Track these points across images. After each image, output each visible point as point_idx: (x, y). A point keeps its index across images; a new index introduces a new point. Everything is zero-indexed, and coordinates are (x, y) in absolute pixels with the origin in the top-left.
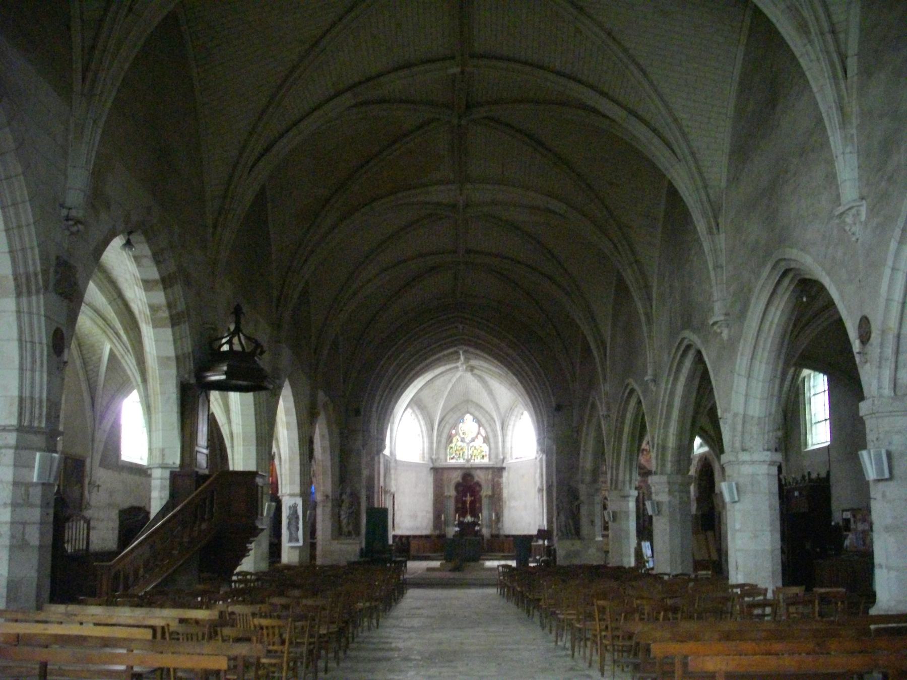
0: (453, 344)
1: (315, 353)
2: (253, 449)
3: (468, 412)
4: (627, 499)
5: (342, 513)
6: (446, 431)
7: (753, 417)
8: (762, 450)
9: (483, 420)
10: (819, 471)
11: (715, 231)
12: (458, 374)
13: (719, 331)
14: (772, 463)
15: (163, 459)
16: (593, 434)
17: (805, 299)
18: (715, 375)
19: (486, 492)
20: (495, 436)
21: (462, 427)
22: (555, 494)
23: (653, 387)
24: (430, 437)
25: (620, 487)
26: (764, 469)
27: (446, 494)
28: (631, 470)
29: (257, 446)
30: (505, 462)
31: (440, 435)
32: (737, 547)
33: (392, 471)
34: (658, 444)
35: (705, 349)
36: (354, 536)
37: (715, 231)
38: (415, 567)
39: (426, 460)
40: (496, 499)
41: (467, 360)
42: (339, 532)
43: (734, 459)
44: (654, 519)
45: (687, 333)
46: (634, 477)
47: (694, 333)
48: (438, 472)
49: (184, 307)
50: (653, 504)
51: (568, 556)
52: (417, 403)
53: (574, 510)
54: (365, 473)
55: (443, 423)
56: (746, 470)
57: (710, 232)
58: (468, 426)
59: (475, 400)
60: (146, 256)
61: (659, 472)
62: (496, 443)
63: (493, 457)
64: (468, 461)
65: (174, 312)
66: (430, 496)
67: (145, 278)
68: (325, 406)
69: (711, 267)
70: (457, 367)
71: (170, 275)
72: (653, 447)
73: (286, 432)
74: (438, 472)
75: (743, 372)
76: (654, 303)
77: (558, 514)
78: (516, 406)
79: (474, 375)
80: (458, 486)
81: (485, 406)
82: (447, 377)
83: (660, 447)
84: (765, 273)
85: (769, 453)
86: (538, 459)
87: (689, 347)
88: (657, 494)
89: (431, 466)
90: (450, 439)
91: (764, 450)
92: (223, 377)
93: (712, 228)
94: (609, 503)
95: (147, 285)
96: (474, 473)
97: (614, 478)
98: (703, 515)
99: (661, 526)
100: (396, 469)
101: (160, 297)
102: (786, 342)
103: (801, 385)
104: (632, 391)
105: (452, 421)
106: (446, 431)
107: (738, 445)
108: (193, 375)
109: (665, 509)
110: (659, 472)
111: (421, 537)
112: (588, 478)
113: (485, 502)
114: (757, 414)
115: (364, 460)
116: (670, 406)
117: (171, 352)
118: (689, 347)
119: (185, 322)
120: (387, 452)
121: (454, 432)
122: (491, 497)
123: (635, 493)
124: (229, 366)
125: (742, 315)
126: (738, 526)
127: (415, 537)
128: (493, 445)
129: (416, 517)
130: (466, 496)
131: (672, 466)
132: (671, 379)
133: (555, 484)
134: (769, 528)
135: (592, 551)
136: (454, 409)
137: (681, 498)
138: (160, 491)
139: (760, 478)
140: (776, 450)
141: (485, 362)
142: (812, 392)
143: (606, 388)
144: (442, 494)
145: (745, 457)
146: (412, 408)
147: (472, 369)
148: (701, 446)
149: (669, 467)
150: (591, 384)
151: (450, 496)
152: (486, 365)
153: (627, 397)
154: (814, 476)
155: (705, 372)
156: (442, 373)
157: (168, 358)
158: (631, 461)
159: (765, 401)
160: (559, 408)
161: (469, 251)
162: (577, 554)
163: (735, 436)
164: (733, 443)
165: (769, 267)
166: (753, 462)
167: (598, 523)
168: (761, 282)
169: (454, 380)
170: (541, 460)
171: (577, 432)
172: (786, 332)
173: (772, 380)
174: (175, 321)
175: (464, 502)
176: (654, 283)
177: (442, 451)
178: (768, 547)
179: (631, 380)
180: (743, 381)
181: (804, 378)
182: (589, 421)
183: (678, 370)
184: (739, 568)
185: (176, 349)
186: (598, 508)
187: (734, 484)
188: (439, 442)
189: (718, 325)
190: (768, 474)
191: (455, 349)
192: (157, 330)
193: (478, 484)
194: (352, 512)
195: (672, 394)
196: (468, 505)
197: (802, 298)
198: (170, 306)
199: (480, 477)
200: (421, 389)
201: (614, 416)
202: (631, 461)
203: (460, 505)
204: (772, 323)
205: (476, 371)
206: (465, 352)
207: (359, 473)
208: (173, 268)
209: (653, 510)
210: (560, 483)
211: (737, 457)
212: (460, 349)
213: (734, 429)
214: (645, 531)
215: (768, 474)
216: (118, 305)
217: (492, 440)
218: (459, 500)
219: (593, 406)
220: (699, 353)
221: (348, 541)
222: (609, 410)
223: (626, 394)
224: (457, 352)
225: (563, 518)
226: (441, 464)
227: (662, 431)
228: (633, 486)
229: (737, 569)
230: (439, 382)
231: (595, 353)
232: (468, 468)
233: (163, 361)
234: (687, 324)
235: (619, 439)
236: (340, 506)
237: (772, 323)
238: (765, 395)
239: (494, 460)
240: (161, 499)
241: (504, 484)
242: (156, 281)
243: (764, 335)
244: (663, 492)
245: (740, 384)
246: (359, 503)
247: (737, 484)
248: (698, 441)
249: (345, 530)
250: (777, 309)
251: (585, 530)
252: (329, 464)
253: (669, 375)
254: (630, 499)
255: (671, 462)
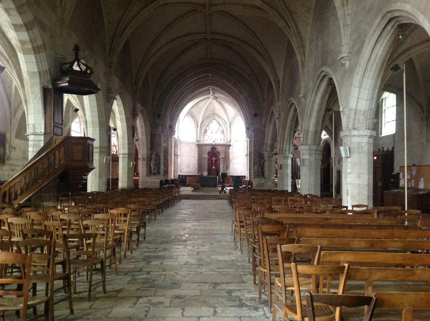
0: (206, 85)
1: (135, 84)
2: (98, 129)
3: (215, 119)
4: (287, 158)
5: (152, 164)
6: (204, 128)
7: (361, 111)
8: (365, 129)
9: (221, 123)
10: (388, 147)
11: (345, 4)
12: (210, 100)
13: (344, 62)
14: (370, 137)
15: (34, 130)
16: (271, 127)
17: (400, 37)
18: (339, 89)
19: (222, 156)
20: (227, 130)
21: (211, 126)
22: (252, 156)
23: (303, 100)
24: (197, 130)
25: (284, 153)
26: (366, 140)
27: (204, 157)
28: (290, 144)
29: (100, 127)
30: (231, 142)
31: (201, 130)
32: (348, 182)
33: (179, 146)
34: (304, 130)
35: (335, 76)
36: (157, 175)
37: (345, 4)
38: (186, 190)
39: (195, 141)
40: (227, 159)
41: (214, 93)
42: (150, 173)
43: (349, 134)
44: (301, 168)
45: (325, 69)
46: (291, 148)
47: (328, 67)
48: (200, 146)
49: (41, 43)
50: (300, 160)
51: (258, 185)
52: (190, 113)
53: (262, 164)
54: (164, 145)
55: (203, 124)
56: (356, 140)
57: (343, 5)
58: (214, 126)
59: (217, 113)
60: (12, 9)
61: (304, 144)
62: (227, 133)
63: (225, 140)
64: (214, 141)
65: (35, 46)
66: (197, 158)
67: (15, 23)
68: (141, 112)
69: (341, 26)
70: (209, 97)
71: (29, 22)
72: (302, 131)
73: (120, 123)
74: (200, 146)
75: (357, 85)
76: (306, 55)
77: (254, 166)
78: (237, 117)
79: (217, 101)
80: (209, 153)
81: (220, 115)
82: (205, 102)
83: (305, 131)
84: (377, 22)
85: (369, 131)
86: (246, 141)
87: (325, 76)
88: (303, 155)
89: (197, 143)
90: (206, 131)
91: (366, 129)
92: (67, 84)
93: (344, 3)
94: (278, 161)
95: (16, 27)
96: (217, 147)
97: (281, 148)
98: (324, 169)
99: (304, 172)
100: (180, 145)
101: (25, 36)
102: (384, 67)
103: (381, 103)
104: (292, 104)
105: (207, 123)
106: (204, 128)
107: (351, 126)
108: (50, 83)
109: (307, 163)
110: (304, 144)
111: (191, 176)
112: (268, 149)
113: (221, 161)
114: (363, 109)
115: (162, 140)
116: (312, 109)
117: (36, 69)
118: (325, 76)
119: (42, 51)
120: (175, 136)
121: (207, 128)
122: (224, 158)
123: (292, 156)
124: (69, 78)
125: (359, 52)
126: (349, 171)
127: (189, 176)
128: (225, 135)
129: (190, 167)
130: (213, 158)
131: (311, 141)
132: (314, 94)
133: (253, 152)
134: (367, 173)
135: (270, 183)
136: (208, 117)
137: (315, 157)
138: (33, 148)
139: (363, 145)
140: (373, 129)
141: (222, 94)
142: (387, 106)
143: (278, 104)
144: (202, 157)
145: (355, 133)
146: (187, 116)
147: (216, 98)
148: (325, 135)
149: (310, 141)
150: (272, 103)
151: (205, 158)
152: (223, 96)
153: (289, 108)
154: (385, 149)
155: (334, 88)
156: (202, 100)
157: (34, 73)
158: (290, 140)
159: (369, 101)
160: (255, 115)
161: (212, 33)
162: (262, 185)
163: (350, 121)
164: (348, 126)
165: (380, 18)
166: (359, 136)
167: (274, 170)
168: (372, 30)
169: (208, 104)
170: (247, 141)
171: (264, 127)
172: (385, 59)
173: (374, 90)
174: (36, 50)
175: (212, 161)
176: (307, 44)
177: (202, 137)
178: (366, 183)
179: (292, 99)
180: (357, 90)
181: (383, 99)
182: (270, 121)
183: (317, 91)
184: (349, 193)
185: (38, 68)
186: (274, 163)
187: (348, 147)
188: (201, 133)
189: (343, 59)
190: (368, 143)
191: (207, 88)
192: (26, 56)
193: (218, 152)
194: (157, 163)
195: (314, 102)
196: (214, 162)
197: (399, 36)
198: (31, 41)
199: (219, 149)
200: (192, 107)
201: (282, 116)
202: (290, 140)
203: (210, 162)
204: (377, 54)
205: (218, 100)
206: (213, 89)
207: (160, 145)
208: (30, 17)
209: (301, 163)
210: (255, 151)
211: (350, 132)
212: (211, 87)
213: (349, 118)
214: (296, 175)
215: (368, 143)
216: (3, 42)
217: (225, 132)
218: (210, 159)
219: (273, 113)
220: (331, 79)
221: (154, 177)
222: (280, 115)
223: (289, 106)
224: (209, 89)
225: (256, 167)
226: (201, 143)
227: (307, 123)
228: (291, 152)
229: (347, 194)
230: (201, 104)
231: (274, 86)
232: (214, 145)
233: (31, 74)
234: (324, 63)
235: (284, 129)
236: (151, 161)
237: (377, 54)
238: (369, 98)
239: (226, 141)
240: (34, 152)
241: (230, 153)
242: (21, 25)
243: (371, 62)
244: (306, 154)
245: (355, 92)
246: (160, 160)
247: (349, 148)
248: (324, 132)
249: (153, 172)
250: (381, 45)
251: (266, 174)
252: (145, 140)
253: (312, 93)
254: (289, 158)
255: (311, 139)
